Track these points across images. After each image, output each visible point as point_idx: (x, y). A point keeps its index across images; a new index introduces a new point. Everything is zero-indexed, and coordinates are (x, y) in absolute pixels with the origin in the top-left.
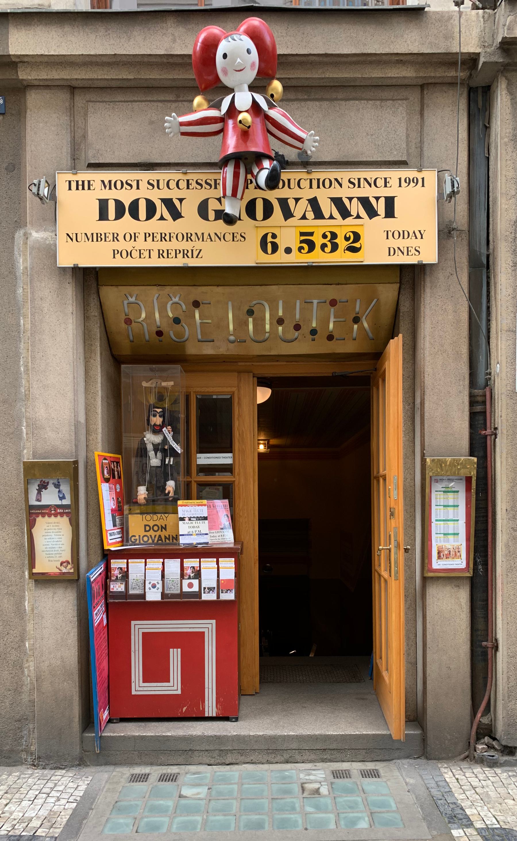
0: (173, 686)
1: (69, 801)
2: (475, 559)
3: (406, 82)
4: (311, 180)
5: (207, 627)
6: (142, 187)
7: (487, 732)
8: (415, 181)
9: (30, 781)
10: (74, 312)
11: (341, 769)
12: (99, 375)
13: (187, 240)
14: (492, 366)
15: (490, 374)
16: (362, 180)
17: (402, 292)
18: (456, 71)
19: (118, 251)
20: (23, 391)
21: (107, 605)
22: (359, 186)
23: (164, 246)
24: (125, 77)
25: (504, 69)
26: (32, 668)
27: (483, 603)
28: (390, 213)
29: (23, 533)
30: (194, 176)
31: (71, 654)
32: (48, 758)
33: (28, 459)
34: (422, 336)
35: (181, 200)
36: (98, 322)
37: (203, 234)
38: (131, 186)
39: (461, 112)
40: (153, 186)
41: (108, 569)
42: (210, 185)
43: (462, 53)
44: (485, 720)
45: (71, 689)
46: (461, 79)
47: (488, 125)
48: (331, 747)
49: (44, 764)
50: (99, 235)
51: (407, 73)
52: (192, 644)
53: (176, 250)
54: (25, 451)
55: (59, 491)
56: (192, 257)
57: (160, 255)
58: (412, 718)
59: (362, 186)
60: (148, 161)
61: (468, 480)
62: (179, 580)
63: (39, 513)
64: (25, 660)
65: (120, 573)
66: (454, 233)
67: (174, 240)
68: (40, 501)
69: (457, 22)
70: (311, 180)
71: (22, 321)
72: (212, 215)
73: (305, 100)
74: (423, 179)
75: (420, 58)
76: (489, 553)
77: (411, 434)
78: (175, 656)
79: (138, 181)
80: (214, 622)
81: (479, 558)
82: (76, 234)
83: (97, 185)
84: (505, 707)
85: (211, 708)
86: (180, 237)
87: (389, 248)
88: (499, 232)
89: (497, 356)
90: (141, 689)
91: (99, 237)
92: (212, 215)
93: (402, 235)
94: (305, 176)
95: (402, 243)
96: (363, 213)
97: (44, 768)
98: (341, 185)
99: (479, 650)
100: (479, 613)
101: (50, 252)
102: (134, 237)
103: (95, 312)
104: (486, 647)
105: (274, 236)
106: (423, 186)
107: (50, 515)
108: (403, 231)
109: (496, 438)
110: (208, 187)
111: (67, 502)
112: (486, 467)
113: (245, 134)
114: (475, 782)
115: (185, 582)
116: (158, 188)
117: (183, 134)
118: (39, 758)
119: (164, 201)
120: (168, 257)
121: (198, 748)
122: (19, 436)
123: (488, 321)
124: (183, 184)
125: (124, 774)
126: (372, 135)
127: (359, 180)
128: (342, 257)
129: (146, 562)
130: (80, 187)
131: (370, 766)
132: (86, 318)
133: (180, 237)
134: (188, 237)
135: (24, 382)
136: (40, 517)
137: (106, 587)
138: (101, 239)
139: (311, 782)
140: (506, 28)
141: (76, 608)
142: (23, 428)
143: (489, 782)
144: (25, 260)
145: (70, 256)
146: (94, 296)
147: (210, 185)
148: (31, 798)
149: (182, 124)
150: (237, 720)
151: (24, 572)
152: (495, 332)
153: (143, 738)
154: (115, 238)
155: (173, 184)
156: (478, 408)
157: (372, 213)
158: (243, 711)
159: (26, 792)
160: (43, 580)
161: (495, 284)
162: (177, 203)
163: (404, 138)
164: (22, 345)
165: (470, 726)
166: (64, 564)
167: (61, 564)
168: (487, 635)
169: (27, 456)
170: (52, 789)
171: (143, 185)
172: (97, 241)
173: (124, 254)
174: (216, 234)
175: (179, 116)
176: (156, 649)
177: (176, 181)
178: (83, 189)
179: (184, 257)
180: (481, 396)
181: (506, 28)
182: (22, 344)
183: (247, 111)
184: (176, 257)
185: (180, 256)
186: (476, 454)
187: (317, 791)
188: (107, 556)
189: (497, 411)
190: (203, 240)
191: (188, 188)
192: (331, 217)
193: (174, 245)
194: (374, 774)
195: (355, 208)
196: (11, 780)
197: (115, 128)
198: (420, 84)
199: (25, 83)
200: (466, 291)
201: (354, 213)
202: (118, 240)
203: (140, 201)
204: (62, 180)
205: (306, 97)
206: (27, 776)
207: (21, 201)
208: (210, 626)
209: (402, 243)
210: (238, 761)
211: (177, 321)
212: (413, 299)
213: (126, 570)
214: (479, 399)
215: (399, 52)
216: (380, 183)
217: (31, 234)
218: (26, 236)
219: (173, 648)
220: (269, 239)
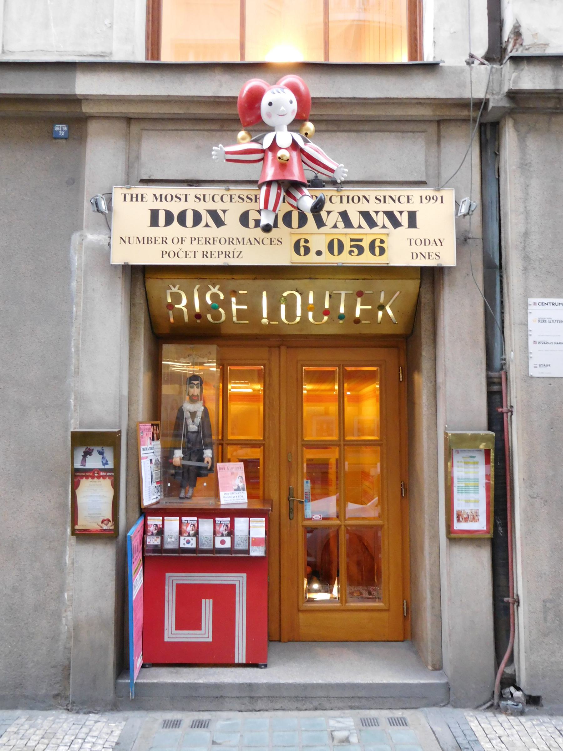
0: (205, 634)
1: (105, 746)
2: (495, 521)
3: (425, 118)
4: (341, 197)
5: (239, 580)
6: (189, 200)
7: (510, 681)
8: (435, 198)
9: (65, 726)
10: (123, 302)
11: (368, 717)
12: (142, 353)
13: (229, 244)
14: (507, 353)
15: (505, 360)
16: (387, 198)
17: (423, 286)
18: (469, 111)
19: (166, 252)
20: (73, 368)
21: (143, 557)
22: (385, 202)
23: (208, 248)
24: (176, 112)
25: (510, 112)
26: (69, 618)
27: (503, 562)
28: (412, 223)
29: (67, 494)
30: (236, 191)
31: (108, 605)
32: (83, 703)
33: (75, 428)
34: (442, 326)
35: (224, 211)
36: (143, 308)
37: (243, 239)
38: (180, 199)
39: (475, 139)
40: (199, 199)
41: (145, 525)
42: (251, 200)
43: (474, 99)
44: (509, 671)
45: (108, 639)
46: (473, 117)
47: (497, 153)
48: (359, 695)
49: (77, 708)
50: (150, 239)
52: (224, 597)
53: (219, 252)
54: (72, 421)
55: (103, 458)
56: (233, 257)
57: (204, 255)
58: (437, 667)
59: (387, 201)
60: (195, 179)
61: (487, 453)
62: (212, 537)
63: (84, 476)
64: (64, 610)
65: (156, 529)
66: (470, 241)
67: (217, 243)
68: (85, 465)
69: (468, 75)
70: (341, 197)
71: (75, 309)
73: (335, 131)
74: (442, 197)
75: (437, 102)
76: (509, 517)
77: (433, 409)
78: (207, 606)
79: (186, 195)
80: (245, 575)
81: (498, 521)
82: (129, 238)
83: (149, 197)
84: (527, 659)
85: (240, 656)
86: (223, 241)
87: (412, 253)
88: (510, 241)
89: (511, 345)
90: (174, 636)
91: (149, 240)
92: (252, 223)
93: (424, 242)
94: (335, 193)
95: (424, 249)
96: (388, 223)
97: (78, 712)
98: (368, 201)
99: (502, 605)
100: (501, 570)
101: (105, 252)
102: (181, 241)
103: (140, 300)
104: (508, 603)
105: (306, 241)
106: (442, 202)
107: (93, 477)
108: (425, 240)
109: (512, 414)
110: (249, 201)
111: (110, 466)
112: (504, 440)
113: (283, 165)
114: (500, 731)
115: (218, 539)
116: (204, 201)
117: (228, 160)
118: (73, 702)
119: (208, 211)
120: (211, 257)
121: (229, 695)
122: (68, 408)
123: (502, 313)
124: (226, 198)
125: (157, 720)
126: (394, 160)
127: (385, 197)
128: (367, 259)
130: (134, 199)
131: (399, 713)
132: (132, 304)
133: (223, 241)
134: (230, 241)
135: (74, 361)
136: (84, 479)
137: (143, 541)
138: (152, 242)
139: (340, 729)
140: (511, 82)
141: (114, 563)
142: (71, 400)
143: (514, 731)
144: (80, 257)
145: (122, 255)
146: (139, 284)
147: (251, 200)
148: (67, 743)
149: (227, 153)
150: (266, 666)
151: (66, 529)
152: (508, 324)
153: (174, 685)
154: (164, 241)
155: (217, 198)
156: (495, 388)
157: (396, 224)
158: (271, 658)
159: (62, 737)
160: (84, 536)
161: (508, 284)
162: (221, 214)
163: (423, 162)
164: (74, 330)
165: (494, 676)
166: (105, 522)
167: (102, 522)
168: (509, 591)
169: (75, 426)
170: (87, 734)
171: (191, 198)
172: (148, 243)
173: (172, 254)
174: (255, 239)
175: (224, 146)
176: (189, 599)
177: (220, 196)
178: (137, 200)
179: (226, 257)
180: (497, 378)
181: (511, 82)
182: (74, 328)
183: (286, 149)
184: (219, 257)
185: (222, 256)
186: (494, 428)
187: (346, 740)
188: (145, 512)
189: (512, 391)
190: (243, 244)
191: (231, 201)
192: (360, 227)
193: (217, 247)
194: (402, 722)
195: (381, 219)
196: (46, 725)
197: (167, 153)
198: (437, 118)
199: (87, 115)
200: (482, 292)
201: (380, 223)
202: (166, 243)
203: (187, 212)
204: (118, 194)
205: (336, 129)
206: (61, 720)
207: (77, 208)
208: (241, 579)
209: (424, 249)
210: (267, 708)
212: (433, 293)
213: (161, 526)
214: (496, 380)
215: (418, 97)
216: (404, 200)
217: (86, 236)
218: (83, 238)
219: (205, 598)
220: (302, 243)
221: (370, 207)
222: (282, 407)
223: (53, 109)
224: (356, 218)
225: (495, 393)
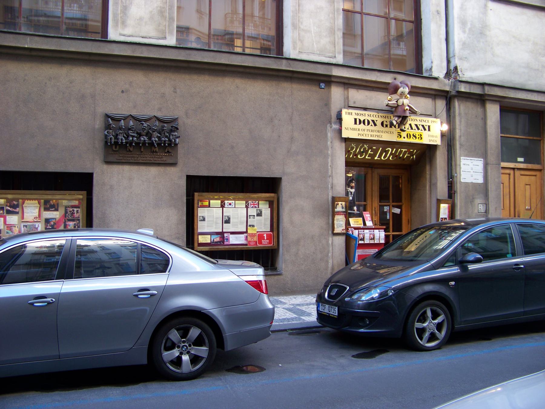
23: (372, 133)
51: (433, 92)
57: (371, 136)
72: (385, 126)
91: (354, 129)
92: (385, 126)
93: (432, 136)
102: (364, 130)
124: (377, 116)
129: (237, 47)
154: (359, 130)
157: (425, 130)
195: (421, 127)
204: (344, 111)
211: (314, 253)
221: (418, 123)
222: (244, 50)
223: (322, 78)
224: (414, 127)
225: (451, 186)
